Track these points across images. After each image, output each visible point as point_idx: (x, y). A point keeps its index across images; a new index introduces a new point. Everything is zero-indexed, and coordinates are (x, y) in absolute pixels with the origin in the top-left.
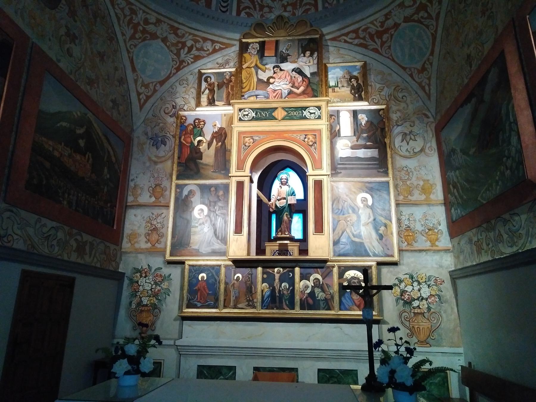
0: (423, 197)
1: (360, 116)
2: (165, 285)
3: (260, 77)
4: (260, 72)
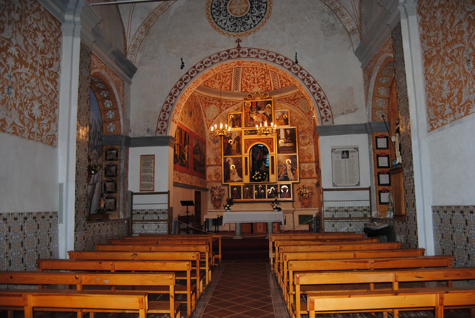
0: (308, 160)
1: (287, 131)
2: (223, 192)
3: (251, 117)
4: (251, 114)
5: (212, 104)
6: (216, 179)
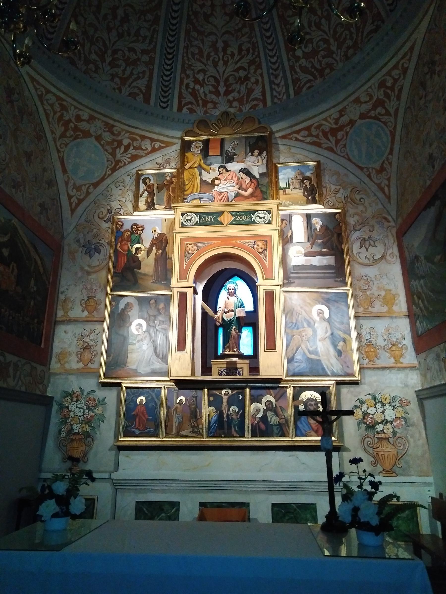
0: (385, 309)
1: (314, 221)
2: (99, 410)
4: (203, 172)
5: (87, 134)
6: (81, 365)
